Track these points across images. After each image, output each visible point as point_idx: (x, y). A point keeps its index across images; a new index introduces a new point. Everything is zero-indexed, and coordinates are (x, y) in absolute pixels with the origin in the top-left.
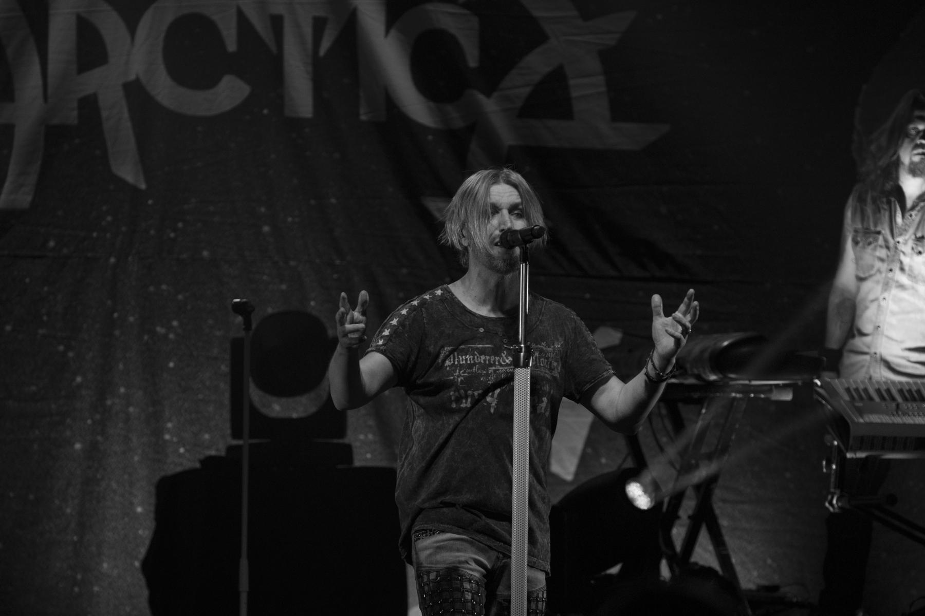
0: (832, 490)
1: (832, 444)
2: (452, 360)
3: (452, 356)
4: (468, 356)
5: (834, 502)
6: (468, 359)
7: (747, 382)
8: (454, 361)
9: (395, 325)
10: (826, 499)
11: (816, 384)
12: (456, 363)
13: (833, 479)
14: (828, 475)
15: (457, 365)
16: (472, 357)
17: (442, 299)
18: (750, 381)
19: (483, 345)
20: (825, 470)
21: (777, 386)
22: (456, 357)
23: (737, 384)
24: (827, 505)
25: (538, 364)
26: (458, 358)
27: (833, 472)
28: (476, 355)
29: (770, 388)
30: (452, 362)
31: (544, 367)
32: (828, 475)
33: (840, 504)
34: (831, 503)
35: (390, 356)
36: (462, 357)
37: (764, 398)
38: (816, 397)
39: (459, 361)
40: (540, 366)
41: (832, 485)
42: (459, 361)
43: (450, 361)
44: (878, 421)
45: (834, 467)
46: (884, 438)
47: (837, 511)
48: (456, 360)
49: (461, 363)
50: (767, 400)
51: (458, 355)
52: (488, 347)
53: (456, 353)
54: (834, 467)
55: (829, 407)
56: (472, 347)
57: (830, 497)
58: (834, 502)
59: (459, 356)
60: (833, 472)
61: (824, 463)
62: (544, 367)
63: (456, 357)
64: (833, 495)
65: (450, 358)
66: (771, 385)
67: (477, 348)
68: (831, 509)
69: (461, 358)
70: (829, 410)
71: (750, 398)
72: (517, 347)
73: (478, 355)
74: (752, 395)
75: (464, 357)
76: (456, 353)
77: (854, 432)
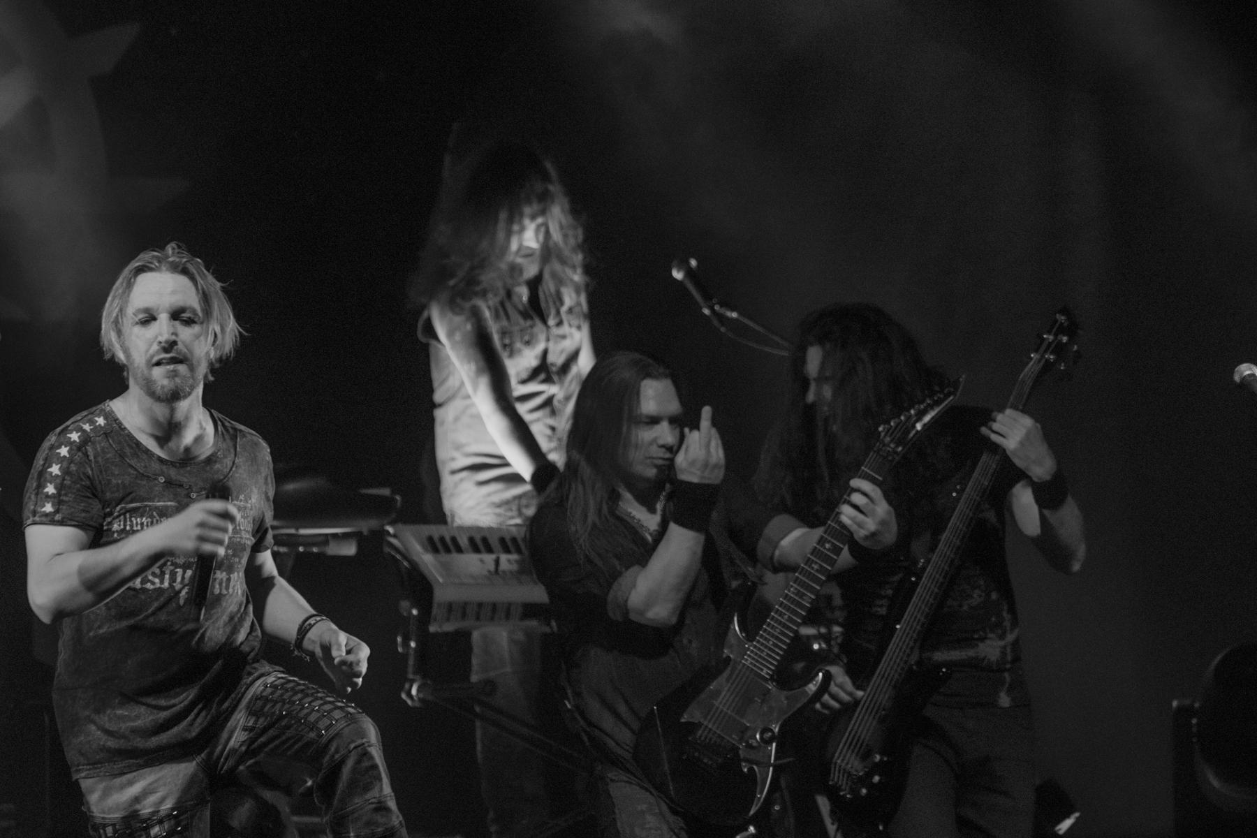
0: (411, 676)
1: (410, 613)
2: (122, 523)
3: (122, 517)
4: (144, 519)
5: (414, 692)
6: (145, 523)
7: (292, 531)
8: (125, 526)
9: (57, 476)
10: (401, 688)
11: (388, 531)
12: (128, 528)
13: (411, 662)
14: (405, 657)
15: (129, 531)
16: (149, 520)
17: (106, 433)
18: (297, 529)
19: (164, 502)
20: (400, 650)
21: (335, 536)
22: (128, 520)
23: (282, 535)
24: (404, 696)
25: (238, 528)
26: (131, 521)
27: (412, 652)
28: (155, 517)
29: (326, 539)
30: (122, 527)
31: (245, 530)
32: (405, 657)
33: (421, 695)
34: (409, 694)
35: (76, 523)
36: (136, 520)
37: (316, 553)
38: (387, 550)
39: (132, 526)
40: (240, 529)
41: (410, 669)
42: (132, 526)
43: (120, 525)
44: (952, 653)
45: (413, 644)
46: (480, 605)
47: (417, 704)
48: (128, 523)
49: (135, 528)
50: (321, 555)
51: (131, 517)
52: (171, 506)
53: (128, 515)
54: (413, 644)
55: (405, 563)
56: (149, 506)
57: (407, 686)
58: (414, 692)
59: (133, 519)
60: (412, 652)
61: (399, 639)
62: (245, 530)
63: (128, 520)
64: (412, 682)
65: (120, 521)
66: (326, 535)
67: (157, 508)
68: (409, 702)
69: (135, 522)
70: (406, 568)
71: (299, 554)
72: (391, 530)
73: (158, 518)
74: (301, 549)
75: (138, 519)
76: (128, 515)
77: (442, 594)
